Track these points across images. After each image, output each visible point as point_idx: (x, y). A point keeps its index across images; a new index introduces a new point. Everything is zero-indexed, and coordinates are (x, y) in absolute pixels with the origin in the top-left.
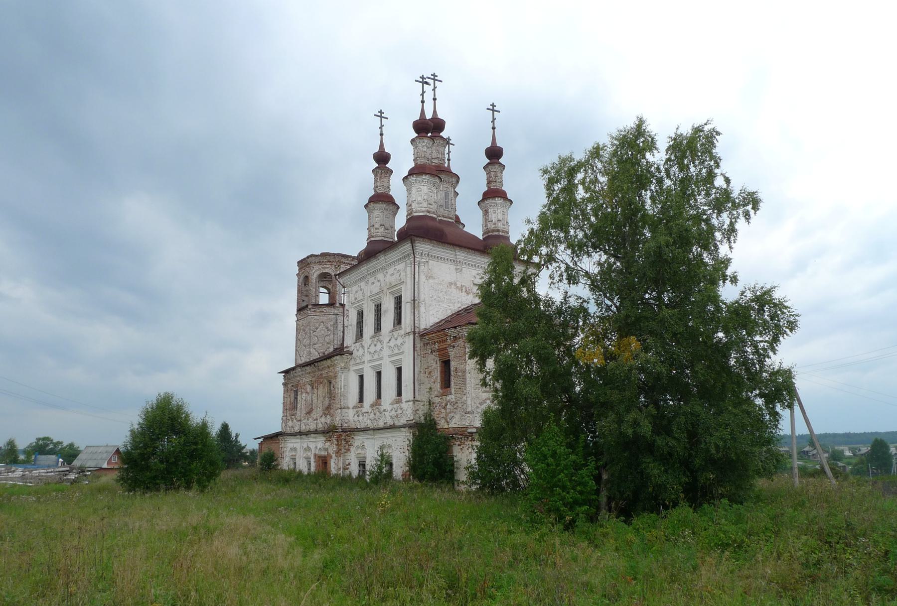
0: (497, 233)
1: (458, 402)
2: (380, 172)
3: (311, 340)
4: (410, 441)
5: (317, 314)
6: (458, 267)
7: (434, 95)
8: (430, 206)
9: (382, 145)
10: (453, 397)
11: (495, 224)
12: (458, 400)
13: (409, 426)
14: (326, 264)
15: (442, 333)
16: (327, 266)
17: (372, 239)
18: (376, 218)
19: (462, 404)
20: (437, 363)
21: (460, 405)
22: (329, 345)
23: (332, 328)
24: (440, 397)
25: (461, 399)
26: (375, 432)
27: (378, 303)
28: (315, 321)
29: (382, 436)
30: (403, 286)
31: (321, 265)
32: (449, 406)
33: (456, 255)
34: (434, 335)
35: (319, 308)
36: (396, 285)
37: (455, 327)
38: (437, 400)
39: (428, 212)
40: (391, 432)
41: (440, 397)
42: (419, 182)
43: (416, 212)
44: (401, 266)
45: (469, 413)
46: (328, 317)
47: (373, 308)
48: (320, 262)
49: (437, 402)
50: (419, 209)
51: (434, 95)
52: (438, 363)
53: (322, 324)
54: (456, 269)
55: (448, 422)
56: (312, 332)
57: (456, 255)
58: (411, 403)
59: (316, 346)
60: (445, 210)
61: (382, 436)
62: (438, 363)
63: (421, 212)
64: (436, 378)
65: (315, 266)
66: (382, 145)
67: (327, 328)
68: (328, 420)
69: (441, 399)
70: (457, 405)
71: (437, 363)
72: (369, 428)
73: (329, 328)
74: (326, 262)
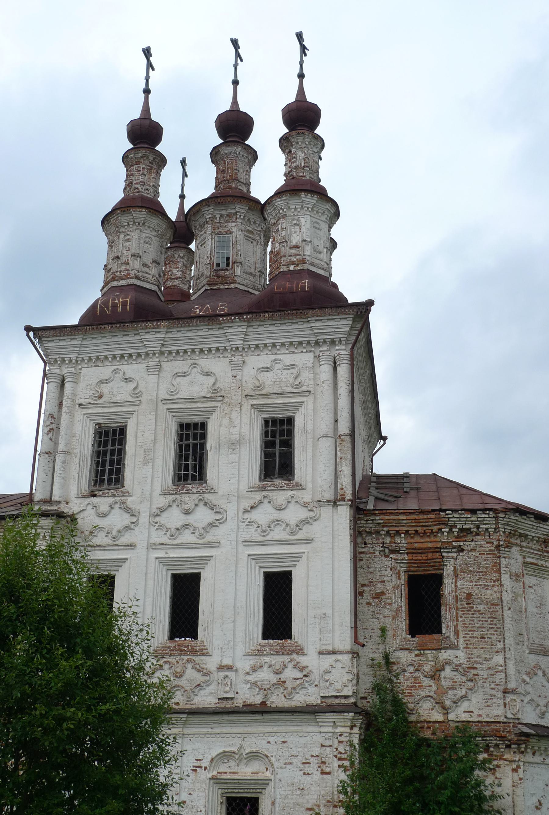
1: (478, 666)
2: (151, 158)
4: (352, 745)
7: (236, 75)
9: (301, 91)
12: (477, 662)
13: (354, 708)
15: (433, 516)
17: (115, 283)
18: (145, 242)
19: (492, 672)
21: (484, 673)
24: (417, 652)
25: (487, 660)
26: (193, 718)
27: (111, 422)
30: (309, 401)
32: (448, 672)
36: (282, 393)
37: (473, 512)
40: (231, 722)
41: (417, 652)
42: (128, 225)
43: (312, 264)
45: (513, 691)
49: (403, 660)
50: (317, 262)
51: (236, 75)
52: (403, 577)
55: (444, 708)
58: (346, 658)
61: (217, 730)
62: (403, 577)
63: (320, 268)
64: (398, 610)
66: (301, 91)
69: (417, 656)
70: (474, 672)
71: (399, 578)
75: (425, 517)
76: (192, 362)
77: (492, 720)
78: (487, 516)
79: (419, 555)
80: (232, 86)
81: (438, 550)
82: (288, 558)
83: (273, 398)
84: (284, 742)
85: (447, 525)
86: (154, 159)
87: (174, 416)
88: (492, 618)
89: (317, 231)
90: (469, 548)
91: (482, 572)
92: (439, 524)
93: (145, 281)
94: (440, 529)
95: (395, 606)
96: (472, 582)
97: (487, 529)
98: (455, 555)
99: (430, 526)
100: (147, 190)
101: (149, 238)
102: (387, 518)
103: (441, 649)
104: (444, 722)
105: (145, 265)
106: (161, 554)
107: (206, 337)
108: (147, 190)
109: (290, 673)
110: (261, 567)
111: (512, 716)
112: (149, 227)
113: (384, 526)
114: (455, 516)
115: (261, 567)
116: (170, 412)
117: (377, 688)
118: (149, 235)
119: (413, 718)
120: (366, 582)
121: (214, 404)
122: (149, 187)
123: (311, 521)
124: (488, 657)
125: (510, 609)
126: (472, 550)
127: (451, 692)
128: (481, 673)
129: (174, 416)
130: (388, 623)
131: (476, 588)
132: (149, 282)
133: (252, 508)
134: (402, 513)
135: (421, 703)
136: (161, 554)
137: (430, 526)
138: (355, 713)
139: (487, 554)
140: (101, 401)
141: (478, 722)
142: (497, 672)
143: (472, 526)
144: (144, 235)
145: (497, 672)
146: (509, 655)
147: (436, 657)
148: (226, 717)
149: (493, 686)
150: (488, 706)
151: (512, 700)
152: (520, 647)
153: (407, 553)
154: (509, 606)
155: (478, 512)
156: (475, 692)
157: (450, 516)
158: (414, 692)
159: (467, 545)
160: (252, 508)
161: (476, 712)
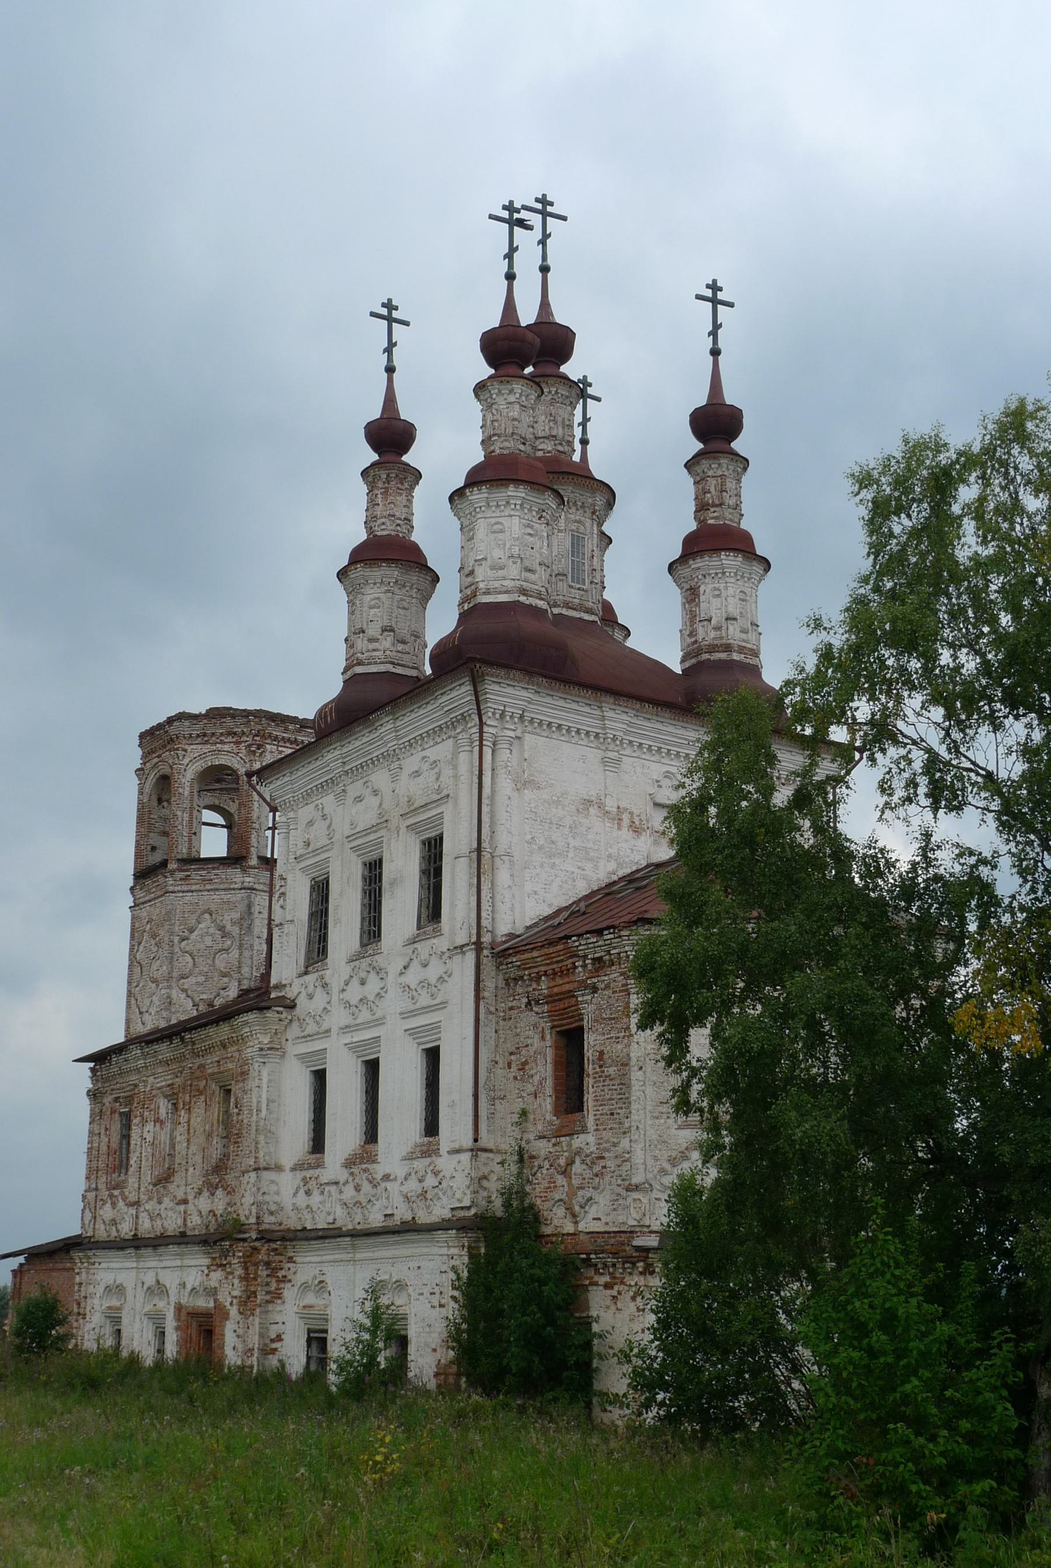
0: (723, 656)
1: (606, 1155)
3: (175, 963)
5: (194, 887)
6: (610, 754)
7: (544, 257)
8: (529, 575)
10: (591, 1138)
11: (718, 628)
14: (222, 742)
16: (226, 747)
17: (359, 670)
18: (371, 608)
20: (543, 1038)
21: (611, 1164)
22: (226, 980)
23: (235, 930)
25: (615, 1145)
27: (373, 856)
28: (187, 908)
29: (377, 1255)
31: (206, 742)
32: (577, 1167)
33: (603, 718)
34: (535, 954)
35: (198, 869)
37: (599, 932)
38: (542, 1148)
39: (523, 592)
40: (397, 1243)
41: (554, 1140)
43: (487, 592)
44: (442, 750)
46: (226, 896)
47: (357, 871)
48: (205, 735)
50: (497, 584)
51: (544, 257)
52: (548, 1037)
53: (207, 916)
54: (604, 761)
56: (176, 939)
57: (603, 718)
58: (466, 1157)
59: (187, 983)
60: (571, 587)
61: (377, 1255)
62: (548, 1037)
63: (500, 593)
65: (189, 748)
67: (222, 928)
68: (219, 1203)
70: (602, 1163)
71: (543, 1038)
72: (340, 1228)
73: (229, 927)
74: (222, 734)
75: (555, 949)
76: (365, 779)
77: (617, 1229)
78: (612, 936)
79: (557, 1003)
80: (395, 363)
81: (570, 994)
82: (433, 1029)
83: (422, 812)
84: (419, 1268)
85: (578, 956)
86: (388, 475)
87: (358, 856)
88: (622, 1084)
89: (500, 536)
90: (603, 986)
91: (613, 1019)
92: (571, 957)
93: (369, 664)
94: (574, 963)
95: (537, 1078)
96: (604, 1034)
97: (619, 954)
98: (589, 997)
99: (562, 961)
100: (383, 524)
101: (378, 598)
102: (523, 957)
103: (573, 1134)
104: (574, 1234)
105: (371, 640)
106: (347, 1039)
107: (370, 743)
108: (383, 524)
109: (431, 1181)
110: (419, 1044)
111: (635, 1223)
112: (375, 584)
113: (525, 969)
114: (583, 942)
115: (419, 1044)
116: (355, 851)
117: (508, 1195)
118: (376, 595)
119: (547, 1230)
120: (513, 1049)
121: (378, 835)
122: (383, 520)
123: (446, 978)
124: (615, 1140)
125: (641, 1068)
126: (607, 987)
127: (580, 1193)
128: (609, 1164)
129: (358, 856)
130: (532, 1105)
131: (607, 1042)
132: (376, 663)
133: (405, 968)
134: (532, 949)
135: (554, 1209)
136: (347, 1039)
137: (562, 961)
138: (458, 1229)
139: (621, 991)
140: (310, 849)
141: (606, 1232)
142: (623, 1161)
143: (603, 954)
144: (368, 598)
145: (623, 1161)
146: (637, 1137)
147: (570, 1145)
148: (370, 1241)
149: (619, 1182)
150: (615, 1210)
151: (635, 1200)
152: (662, 1121)
153: (547, 1003)
154: (641, 1064)
155: (606, 932)
156: (603, 1191)
157: (577, 944)
158: (549, 1195)
159: (601, 981)
160: (405, 968)
161: (604, 1220)
